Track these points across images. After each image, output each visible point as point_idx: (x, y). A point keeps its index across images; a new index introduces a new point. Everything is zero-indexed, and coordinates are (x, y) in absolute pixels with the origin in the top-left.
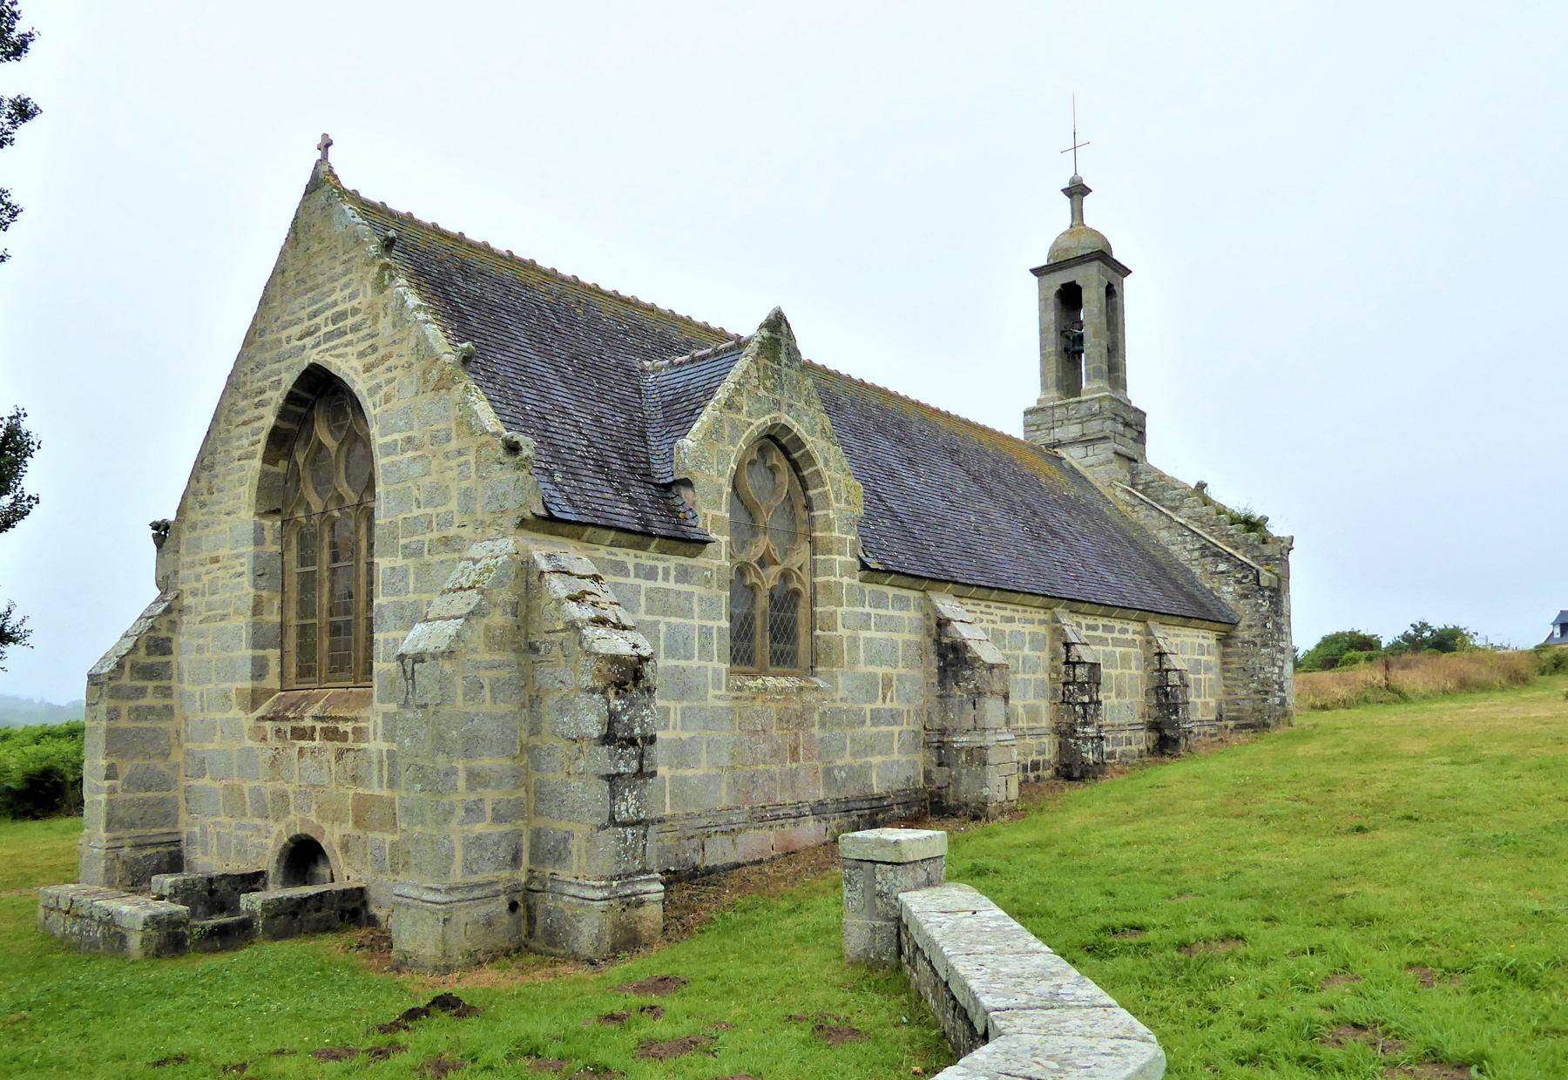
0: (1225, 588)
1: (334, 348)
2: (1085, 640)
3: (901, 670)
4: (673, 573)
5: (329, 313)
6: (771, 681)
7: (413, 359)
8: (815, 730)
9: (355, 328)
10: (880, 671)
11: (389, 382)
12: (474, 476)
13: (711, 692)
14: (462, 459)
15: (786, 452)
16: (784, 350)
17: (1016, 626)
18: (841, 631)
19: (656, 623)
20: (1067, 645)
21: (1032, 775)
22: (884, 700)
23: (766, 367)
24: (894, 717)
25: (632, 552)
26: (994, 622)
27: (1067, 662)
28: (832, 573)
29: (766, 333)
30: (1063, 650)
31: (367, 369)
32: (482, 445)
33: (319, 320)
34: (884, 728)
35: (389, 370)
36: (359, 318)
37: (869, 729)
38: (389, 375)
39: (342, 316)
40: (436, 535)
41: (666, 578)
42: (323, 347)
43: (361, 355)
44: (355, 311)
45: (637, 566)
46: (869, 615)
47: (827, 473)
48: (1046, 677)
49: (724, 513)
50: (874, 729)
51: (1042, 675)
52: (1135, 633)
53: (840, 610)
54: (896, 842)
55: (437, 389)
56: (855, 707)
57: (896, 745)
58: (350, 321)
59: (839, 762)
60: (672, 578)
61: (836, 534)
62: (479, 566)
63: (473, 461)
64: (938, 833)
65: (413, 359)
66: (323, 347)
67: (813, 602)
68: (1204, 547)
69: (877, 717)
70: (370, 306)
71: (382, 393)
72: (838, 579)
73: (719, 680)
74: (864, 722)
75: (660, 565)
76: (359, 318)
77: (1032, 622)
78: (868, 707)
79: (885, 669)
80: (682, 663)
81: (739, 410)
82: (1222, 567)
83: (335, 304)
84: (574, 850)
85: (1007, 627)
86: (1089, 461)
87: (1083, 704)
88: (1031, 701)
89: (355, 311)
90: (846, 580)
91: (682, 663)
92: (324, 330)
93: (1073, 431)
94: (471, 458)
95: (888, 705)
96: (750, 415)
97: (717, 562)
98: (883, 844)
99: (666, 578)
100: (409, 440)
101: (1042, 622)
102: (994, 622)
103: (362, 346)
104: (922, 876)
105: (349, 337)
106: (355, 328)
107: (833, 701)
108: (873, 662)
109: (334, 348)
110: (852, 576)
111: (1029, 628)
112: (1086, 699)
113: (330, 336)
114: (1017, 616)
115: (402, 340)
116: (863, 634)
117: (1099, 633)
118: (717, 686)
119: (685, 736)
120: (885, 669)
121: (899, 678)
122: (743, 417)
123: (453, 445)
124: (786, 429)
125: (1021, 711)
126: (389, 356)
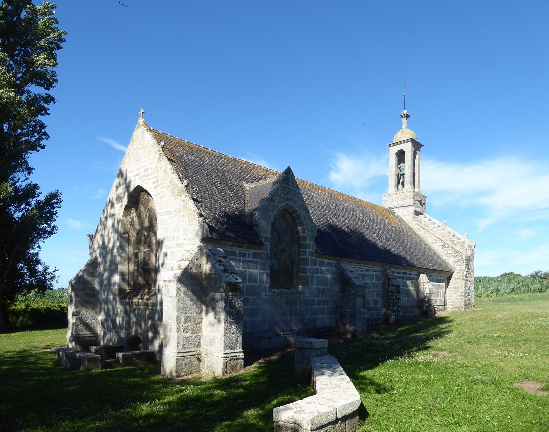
0: (450, 259)
1: (145, 180)
2: (395, 278)
3: (329, 287)
4: (251, 255)
5: (143, 169)
6: (283, 290)
7: (169, 185)
8: (298, 306)
9: (152, 174)
10: (321, 287)
11: (162, 192)
12: (188, 224)
13: (263, 294)
14: (184, 218)
15: (291, 214)
16: (290, 181)
17: (370, 273)
18: (308, 274)
19: (246, 271)
20: (389, 279)
21: (374, 323)
22: (322, 297)
23: (284, 186)
24: (325, 302)
25: (238, 248)
26: (362, 271)
27: (388, 285)
28: (305, 254)
29: (285, 176)
30: (387, 281)
31: (155, 188)
32: (190, 214)
33: (140, 171)
34: (322, 306)
35: (162, 188)
36: (153, 171)
37: (317, 306)
38: (162, 190)
39: (147, 170)
40: (176, 242)
41: (249, 257)
42: (142, 180)
43: (154, 183)
44: (151, 169)
45: (239, 253)
46: (318, 269)
47: (304, 222)
48: (381, 290)
49: (269, 235)
50: (318, 306)
51: (379, 289)
52: (415, 275)
53: (308, 267)
54: (311, 342)
55: (177, 195)
56: (312, 299)
57: (326, 312)
58: (150, 172)
59: (306, 317)
60: (251, 257)
61: (307, 242)
62: (189, 252)
63: (187, 219)
64: (325, 340)
65: (169, 185)
66: (142, 180)
67: (299, 264)
68: (444, 245)
69: (319, 302)
70: (156, 167)
71: (159, 196)
72: (307, 257)
73: (266, 290)
74: (315, 304)
75: (247, 253)
76: (153, 171)
77: (376, 271)
78: (317, 299)
79: (323, 287)
80: (254, 284)
81: (274, 201)
82: (450, 252)
83: (145, 166)
84: (216, 342)
85: (367, 273)
86: (405, 214)
87: (393, 299)
88: (375, 298)
89: (151, 169)
90: (310, 257)
91: (254, 284)
92: (142, 174)
93: (401, 203)
94: (187, 218)
95: (324, 298)
96: (278, 203)
97: (266, 251)
98: (307, 343)
99: (249, 257)
100: (168, 211)
101: (380, 271)
102: (362, 271)
103: (154, 180)
104: (319, 353)
105: (150, 177)
106: (152, 174)
107: (305, 297)
108: (318, 284)
109: (145, 180)
110: (312, 256)
111: (375, 273)
112: (394, 298)
113: (143, 176)
114: (371, 269)
115: (166, 179)
116: (316, 275)
117: (401, 275)
118: (265, 291)
119: (254, 307)
120: (323, 287)
121: (328, 290)
122: (276, 203)
123: (181, 214)
124: (291, 207)
125: (371, 301)
126: (162, 184)
